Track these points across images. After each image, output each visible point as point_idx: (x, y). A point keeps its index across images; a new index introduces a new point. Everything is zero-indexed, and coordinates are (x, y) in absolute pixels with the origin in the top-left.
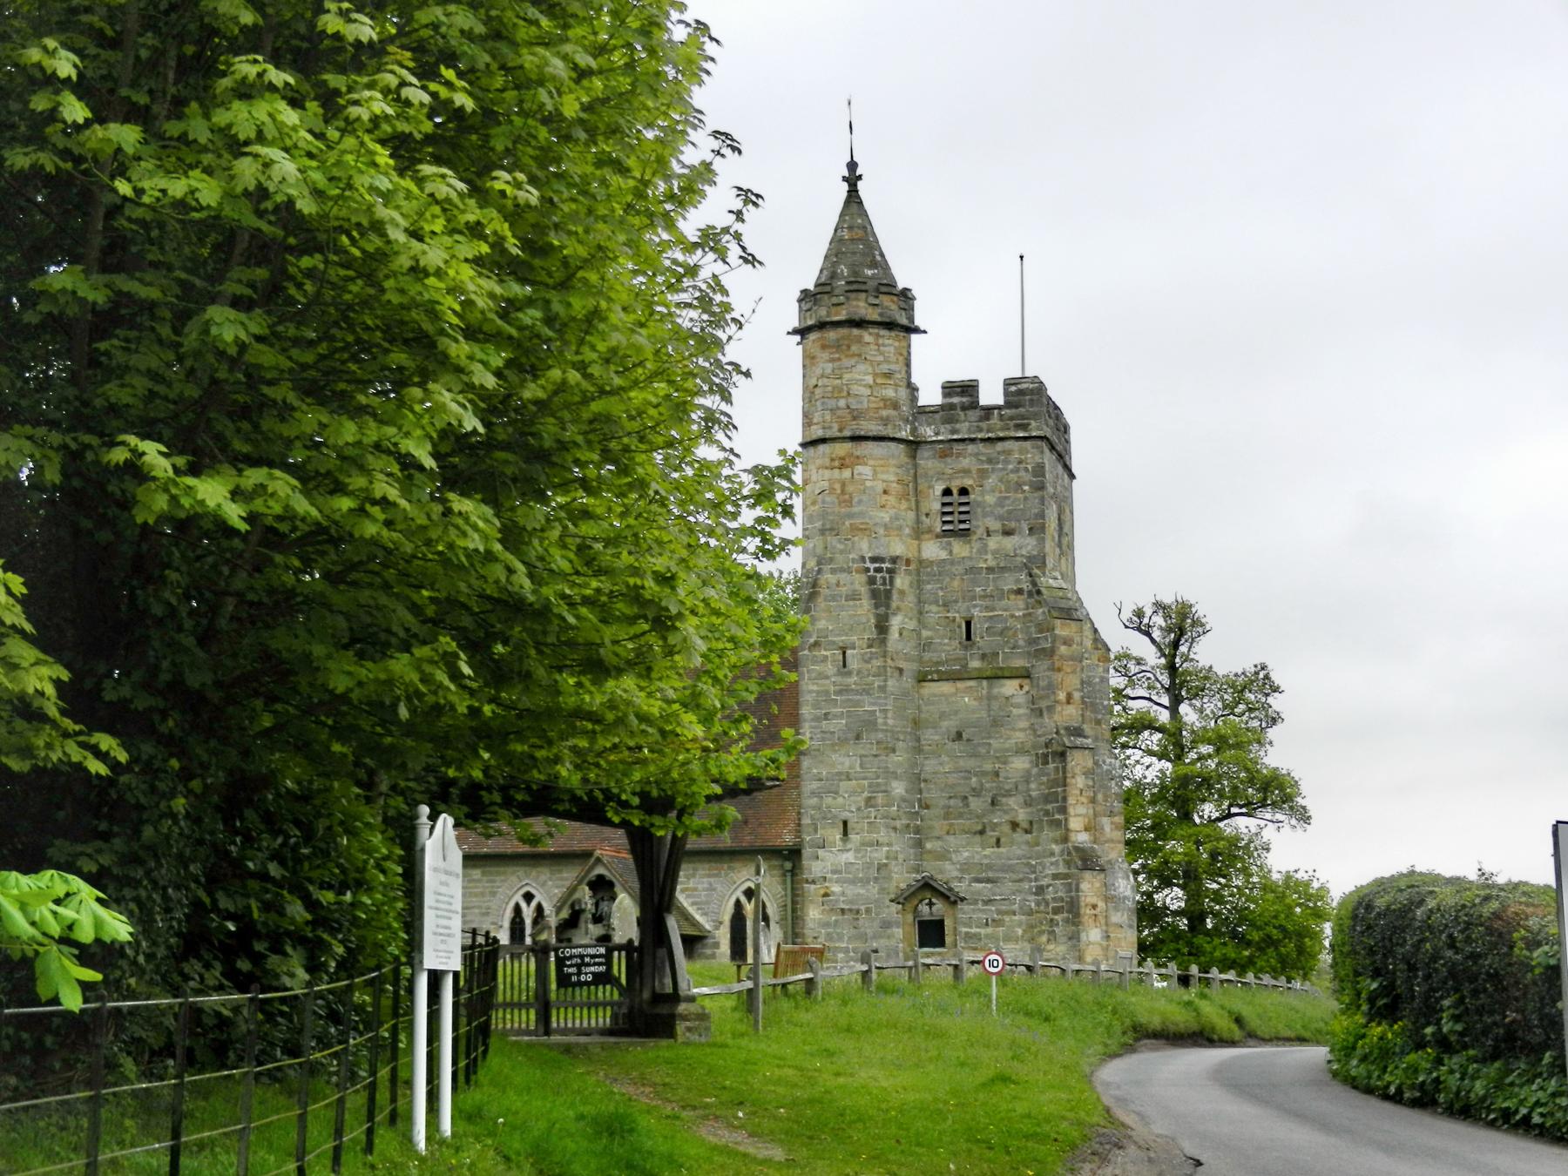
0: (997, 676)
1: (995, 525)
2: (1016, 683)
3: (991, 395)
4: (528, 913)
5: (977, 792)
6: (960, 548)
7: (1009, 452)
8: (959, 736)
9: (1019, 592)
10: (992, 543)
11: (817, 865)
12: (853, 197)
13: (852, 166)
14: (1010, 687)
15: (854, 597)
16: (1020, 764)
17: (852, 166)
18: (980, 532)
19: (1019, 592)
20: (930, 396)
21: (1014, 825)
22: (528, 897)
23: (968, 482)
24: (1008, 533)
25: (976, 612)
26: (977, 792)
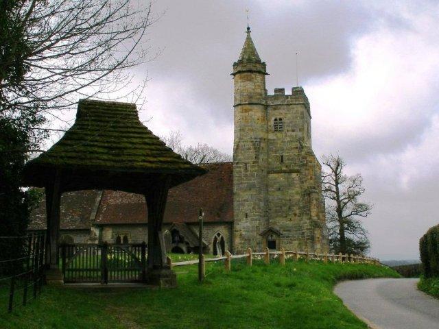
0: (291, 172)
1: (290, 129)
2: (296, 174)
3: (288, 92)
4: (219, 239)
5: (285, 205)
6: (279, 135)
7: (293, 108)
8: (280, 189)
9: (297, 148)
10: (289, 134)
11: (237, 227)
12: (249, 39)
13: (248, 29)
14: (294, 175)
15: (249, 149)
16: (298, 197)
17: (248, 29)
18: (286, 131)
19: (297, 148)
20: (271, 93)
21: (295, 215)
22: (219, 235)
23: (281, 117)
24: (293, 131)
25: (284, 154)
26: (285, 205)
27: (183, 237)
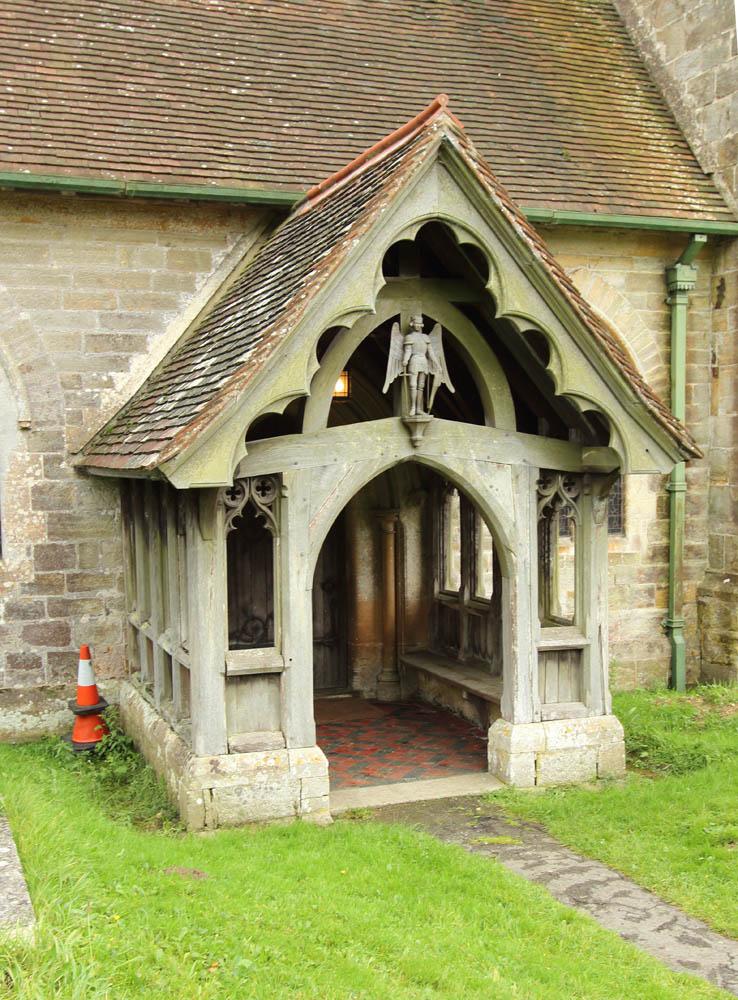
27: (540, 342)
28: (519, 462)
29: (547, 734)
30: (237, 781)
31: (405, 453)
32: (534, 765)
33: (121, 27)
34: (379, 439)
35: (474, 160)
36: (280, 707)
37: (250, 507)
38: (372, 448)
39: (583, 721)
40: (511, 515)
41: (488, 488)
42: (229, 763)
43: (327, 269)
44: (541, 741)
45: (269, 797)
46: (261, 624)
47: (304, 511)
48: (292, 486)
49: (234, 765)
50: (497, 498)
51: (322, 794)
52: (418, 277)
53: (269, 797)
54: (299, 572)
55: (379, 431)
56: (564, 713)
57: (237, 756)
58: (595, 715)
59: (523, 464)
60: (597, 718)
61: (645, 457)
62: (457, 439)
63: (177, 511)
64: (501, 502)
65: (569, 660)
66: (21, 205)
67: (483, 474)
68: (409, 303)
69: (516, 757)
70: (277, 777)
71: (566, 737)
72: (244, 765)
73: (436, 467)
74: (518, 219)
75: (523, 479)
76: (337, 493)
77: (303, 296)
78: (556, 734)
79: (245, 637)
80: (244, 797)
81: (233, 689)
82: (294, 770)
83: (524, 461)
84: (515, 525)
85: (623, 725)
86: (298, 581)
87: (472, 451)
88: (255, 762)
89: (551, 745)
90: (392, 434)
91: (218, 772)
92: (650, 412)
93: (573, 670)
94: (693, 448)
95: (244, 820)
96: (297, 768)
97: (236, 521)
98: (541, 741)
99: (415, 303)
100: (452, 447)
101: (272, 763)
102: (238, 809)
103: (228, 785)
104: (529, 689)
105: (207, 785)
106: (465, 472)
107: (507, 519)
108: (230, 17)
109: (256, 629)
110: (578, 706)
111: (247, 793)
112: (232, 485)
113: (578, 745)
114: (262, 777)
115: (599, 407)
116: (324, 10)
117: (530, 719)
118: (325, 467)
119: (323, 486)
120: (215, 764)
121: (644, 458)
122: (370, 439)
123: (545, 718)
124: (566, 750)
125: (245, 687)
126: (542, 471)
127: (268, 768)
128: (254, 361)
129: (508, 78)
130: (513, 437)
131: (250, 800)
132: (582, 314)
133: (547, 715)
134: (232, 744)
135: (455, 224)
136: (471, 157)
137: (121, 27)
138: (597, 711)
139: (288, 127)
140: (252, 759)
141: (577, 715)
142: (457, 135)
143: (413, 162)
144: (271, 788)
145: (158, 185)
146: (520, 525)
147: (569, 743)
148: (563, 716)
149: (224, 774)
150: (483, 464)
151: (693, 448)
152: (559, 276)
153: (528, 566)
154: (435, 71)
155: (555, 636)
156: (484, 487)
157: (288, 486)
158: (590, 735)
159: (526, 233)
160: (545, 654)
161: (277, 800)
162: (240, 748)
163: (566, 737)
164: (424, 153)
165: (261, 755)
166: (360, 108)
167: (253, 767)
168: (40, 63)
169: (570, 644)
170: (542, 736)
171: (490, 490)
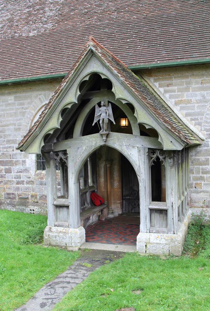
28: (140, 146)
29: (155, 238)
30: (55, 234)
31: (102, 143)
32: (145, 246)
33: (105, 30)
34: (94, 139)
35: (100, 53)
36: (68, 214)
37: (158, 158)
38: (93, 142)
39: (165, 235)
40: (138, 163)
41: (130, 154)
42: (54, 229)
43: (58, 92)
44: (147, 239)
45: (63, 240)
46: (136, 192)
47: (73, 160)
48: (69, 153)
49: (55, 230)
50: (133, 158)
51: (78, 242)
52: (106, 89)
53: (63, 240)
54: (72, 178)
55: (94, 137)
56: (158, 231)
57: (56, 227)
58: (171, 234)
59: (142, 146)
60: (171, 234)
61: (170, 144)
62: (118, 139)
63: (182, 157)
64: (134, 159)
65: (164, 213)
66: (51, 82)
67: (127, 149)
68: (104, 98)
69: (138, 243)
70: (65, 235)
71: (157, 239)
72: (57, 230)
73: (96, 149)
74: (115, 69)
75: (142, 152)
76: (82, 156)
77: (51, 101)
78: (154, 238)
79: (132, 196)
80: (57, 238)
81: (58, 209)
82: (70, 234)
83: (142, 145)
84: (139, 166)
85: (136, 238)
86: (72, 181)
87: (124, 142)
88: (60, 230)
89: (151, 241)
90: (98, 138)
91: (50, 231)
92: (167, 128)
93: (165, 217)
94: (185, 141)
95: (57, 245)
96: (71, 234)
97: (154, 162)
98: (147, 239)
99: (105, 97)
100: (121, 143)
101: (64, 231)
102: (56, 242)
103: (53, 235)
104: (145, 222)
105: (48, 234)
106: (121, 149)
107: (136, 165)
108: (138, 19)
109: (135, 194)
110: (165, 230)
111: (58, 238)
112: (164, 149)
113: (161, 242)
114: (61, 234)
115: (152, 127)
116: (168, 10)
117: (146, 231)
118: (78, 148)
119: (78, 153)
120: (50, 228)
121: (170, 144)
122: (91, 139)
123: (151, 232)
124: (157, 243)
125: (61, 209)
126: (149, 149)
127: (63, 232)
128: (39, 120)
129: (162, 19)
130: (138, 138)
131: (58, 240)
132: (139, 96)
133: (152, 231)
134: (56, 224)
135: (100, 73)
136: (99, 53)
137: (105, 30)
138: (171, 232)
139: (140, 47)
140: (60, 229)
141: (164, 232)
142: (95, 47)
143: (81, 58)
144: (64, 238)
145: (49, 75)
146: (141, 167)
147: (158, 242)
148: (158, 232)
149: (52, 232)
150: (128, 146)
151: (185, 141)
152: (130, 85)
153: (144, 180)
154: (42, 36)
155: (157, 205)
156: (128, 154)
157: (69, 154)
158: (166, 240)
159: (118, 73)
160: (152, 211)
161: (65, 241)
162: (57, 225)
163: (157, 239)
164: (85, 54)
165: (62, 228)
166: (165, 37)
167: (59, 231)
168: (80, 45)
169: (160, 208)
170: (148, 237)
171: (130, 155)
